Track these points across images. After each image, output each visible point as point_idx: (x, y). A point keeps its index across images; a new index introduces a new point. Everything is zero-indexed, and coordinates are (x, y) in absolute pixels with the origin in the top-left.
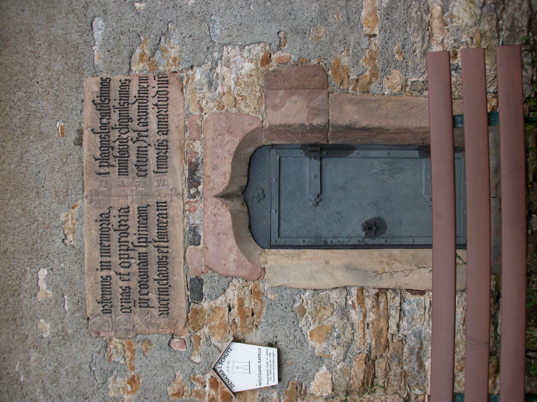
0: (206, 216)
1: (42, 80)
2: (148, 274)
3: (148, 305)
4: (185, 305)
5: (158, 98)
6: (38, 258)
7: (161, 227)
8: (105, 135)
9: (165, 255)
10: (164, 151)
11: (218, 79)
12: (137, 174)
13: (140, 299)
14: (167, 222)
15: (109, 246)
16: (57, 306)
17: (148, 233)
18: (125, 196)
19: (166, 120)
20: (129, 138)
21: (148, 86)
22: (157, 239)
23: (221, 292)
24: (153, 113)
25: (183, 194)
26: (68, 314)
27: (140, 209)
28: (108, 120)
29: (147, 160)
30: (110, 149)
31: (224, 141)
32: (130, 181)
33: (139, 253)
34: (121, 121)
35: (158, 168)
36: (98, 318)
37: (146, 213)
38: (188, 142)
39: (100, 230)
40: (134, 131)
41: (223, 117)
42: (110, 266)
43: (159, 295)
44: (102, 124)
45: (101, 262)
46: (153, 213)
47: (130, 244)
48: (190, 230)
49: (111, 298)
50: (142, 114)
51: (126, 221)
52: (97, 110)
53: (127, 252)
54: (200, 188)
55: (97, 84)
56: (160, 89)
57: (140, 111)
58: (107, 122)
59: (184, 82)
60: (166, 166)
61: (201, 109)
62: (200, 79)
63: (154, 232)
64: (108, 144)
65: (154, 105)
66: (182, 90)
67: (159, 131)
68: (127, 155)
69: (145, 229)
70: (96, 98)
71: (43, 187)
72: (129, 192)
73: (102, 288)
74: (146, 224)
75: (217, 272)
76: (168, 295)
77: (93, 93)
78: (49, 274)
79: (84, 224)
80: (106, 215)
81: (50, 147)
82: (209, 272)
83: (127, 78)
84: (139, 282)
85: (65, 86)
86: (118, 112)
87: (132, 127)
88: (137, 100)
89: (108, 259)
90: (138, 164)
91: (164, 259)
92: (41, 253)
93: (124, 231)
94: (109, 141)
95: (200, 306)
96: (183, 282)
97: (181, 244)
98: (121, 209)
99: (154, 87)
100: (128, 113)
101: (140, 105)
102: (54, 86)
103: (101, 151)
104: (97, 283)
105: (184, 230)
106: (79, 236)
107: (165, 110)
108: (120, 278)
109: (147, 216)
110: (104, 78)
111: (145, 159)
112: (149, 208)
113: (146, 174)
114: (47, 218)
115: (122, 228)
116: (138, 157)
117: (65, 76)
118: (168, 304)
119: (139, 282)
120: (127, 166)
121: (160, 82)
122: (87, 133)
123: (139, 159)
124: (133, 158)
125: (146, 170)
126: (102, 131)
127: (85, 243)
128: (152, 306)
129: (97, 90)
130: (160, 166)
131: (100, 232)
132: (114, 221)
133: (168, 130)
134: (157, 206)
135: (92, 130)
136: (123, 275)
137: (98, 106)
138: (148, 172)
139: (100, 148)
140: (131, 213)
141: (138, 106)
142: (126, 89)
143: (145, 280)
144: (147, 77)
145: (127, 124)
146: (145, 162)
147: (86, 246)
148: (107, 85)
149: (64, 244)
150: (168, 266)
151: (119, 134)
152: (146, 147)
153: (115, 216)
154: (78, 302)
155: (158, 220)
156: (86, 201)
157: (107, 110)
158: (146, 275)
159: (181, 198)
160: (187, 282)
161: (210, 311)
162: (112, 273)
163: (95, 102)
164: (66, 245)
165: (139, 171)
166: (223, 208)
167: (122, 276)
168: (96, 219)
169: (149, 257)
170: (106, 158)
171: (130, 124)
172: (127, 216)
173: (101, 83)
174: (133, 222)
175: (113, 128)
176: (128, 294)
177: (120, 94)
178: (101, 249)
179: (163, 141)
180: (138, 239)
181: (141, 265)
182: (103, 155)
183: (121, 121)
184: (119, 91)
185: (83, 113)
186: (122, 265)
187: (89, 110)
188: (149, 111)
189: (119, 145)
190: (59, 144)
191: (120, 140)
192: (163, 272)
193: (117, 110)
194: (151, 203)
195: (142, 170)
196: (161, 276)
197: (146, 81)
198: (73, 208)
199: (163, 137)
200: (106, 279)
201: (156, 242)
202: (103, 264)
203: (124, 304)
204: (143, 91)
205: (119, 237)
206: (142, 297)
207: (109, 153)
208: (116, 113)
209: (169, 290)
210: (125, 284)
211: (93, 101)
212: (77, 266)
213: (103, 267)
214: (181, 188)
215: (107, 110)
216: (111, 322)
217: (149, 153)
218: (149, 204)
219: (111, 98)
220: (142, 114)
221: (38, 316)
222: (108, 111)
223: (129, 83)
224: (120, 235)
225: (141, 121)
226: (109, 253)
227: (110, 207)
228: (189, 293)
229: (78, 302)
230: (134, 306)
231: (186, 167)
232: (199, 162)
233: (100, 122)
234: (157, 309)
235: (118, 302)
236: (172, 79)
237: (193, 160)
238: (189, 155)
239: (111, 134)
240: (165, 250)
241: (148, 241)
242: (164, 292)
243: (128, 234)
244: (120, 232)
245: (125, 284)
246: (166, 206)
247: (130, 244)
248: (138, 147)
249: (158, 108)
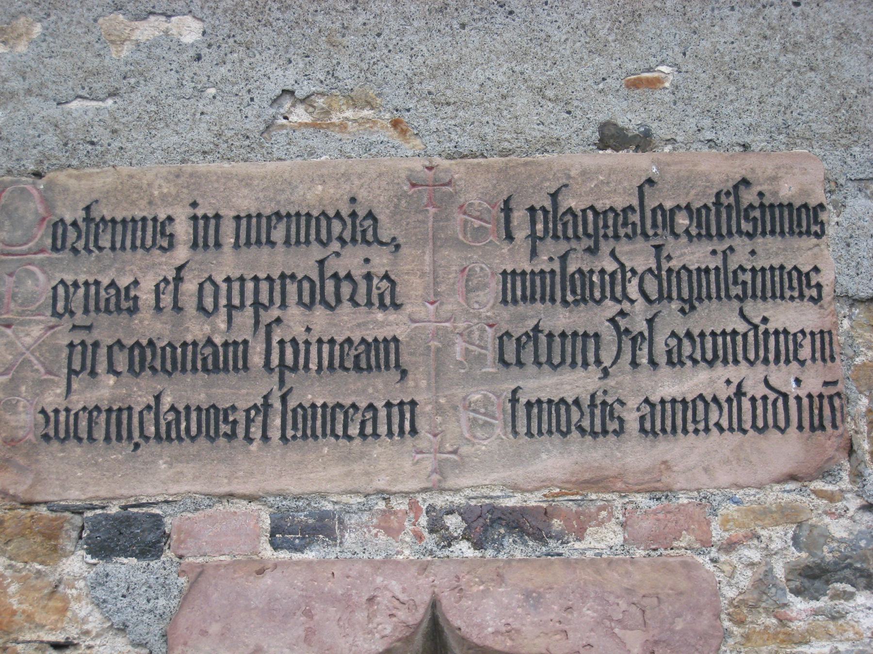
0: (368, 570)
1: (805, 16)
2: (177, 375)
3: (77, 373)
4: (74, 496)
5: (765, 398)
6: (233, 13)
7: (333, 419)
8: (634, 224)
9: (241, 431)
10: (586, 424)
11: (832, 598)
12: (508, 334)
13: (96, 345)
14: (350, 438)
15: (271, 243)
16: (81, 75)
17: (313, 374)
18: (436, 294)
19: (691, 427)
20: (626, 306)
21: (802, 363)
22: (292, 404)
23: (116, 619)
24: (712, 381)
25: (442, 490)
26: (55, 112)
27: (392, 345)
28: (687, 232)
29: (555, 367)
30: (591, 243)
31: (625, 628)
32: (486, 312)
33: (245, 342)
34: (684, 275)
35: (529, 405)
36: (41, 210)
37: (378, 367)
38: (619, 503)
39: (324, 213)
40: (650, 322)
41: (704, 622)
42: (206, 246)
43: (109, 410)
44: (672, 211)
45: (217, 217)
46: (376, 389)
47: (275, 312)
48: (323, 516)
49: (100, 249)
50: (709, 345)
51: (352, 299)
52: (718, 195)
53: (249, 301)
54: (464, 549)
55: (803, 192)
56: (792, 403)
57: (720, 340)
58: (679, 230)
59: (818, 485)
60: (535, 430)
61: (730, 546)
62: (833, 539)
63: (313, 392)
64: (606, 236)
65: (740, 386)
66: (793, 478)
67: (653, 406)
68: (570, 298)
69: (326, 363)
70: (756, 189)
71: (463, 26)
72: (449, 307)
73: (133, 220)
74: (343, 367)
75: (181, 606)
76: (107, 439)
77: (774, 179)
78: (182, 48)
79: (343, 160)
80: (370, 232)
81: (593, 45)
82: (183, 580)
83: (826, 290)
84: (151, 343)
85: (792, 91)
86: (712, 266)
87: (665, 312)
88: (756, 327)
89: (229, 240)
90: (543, 338)
91: (224, 428)
92: (251, 22)
93: (318, 293)
94: (616, 237)
95: (70, 547)
96: (151, 491)
97: (274, 486)
98: (393, 283)
99: (798, 381)
100: (709, 297)
101: (739, 339)
102: (790, 56)
103: (584, 211)
104: (150, 203)
105: (324, 496)
106: (303, 143)
107: (725, 424)
108: (165, 280)
109: (369, 368)
110: (823, 216)
111: (557, 360)
112: (395, 375)
113: (506, 364)
114: (361, 40)
115: (330, 286)
116: (563, 335)
117: (822, 87)
118: (80, 440)
119: (151, 343)
120: (533, 299)
121: (816, 400)
122: (641, 163)
123: (558, 339)
124: (561, 319)
125: (520, 363)
126: (648, 214)
127: (279, 163)
128: (75, 386)
129: (781, 194)
130: (535, 410)
131: (315, 213)
132: (350, 261)
133: (655, 434)
134: (401, 404)
135: (650, 181)
136: (176, 289)
137: (732, 199)
138: (515, 370)
139: (592, 208)
140: (380, 316)
141: (734, 333)
142: (791, 288)
143: (158, 365)
144: (833, 359)
145: (675, 295)
146: (549, 361)
147: (271, 166)
148: (799, 225)
149: (279, 97)
150: (202, 441)
151: (640, 270)
152: (598, 362)
153: (367, 261)
154: (92, 143)
155: (354, 406)
156: (418, 165)
157: (719, 228)
158: (174, 367)
159: (429, 485)
160: (148, 505)
161: (53, 578)
162: (182, 253)
163: (742, 187)
164: (274, 101)
165: (518, 340)
166: (395, 629)
167: (171, 287)
168: (360, 198)
169: (232, 378)
170: (560, 227)
171: (675, 305)
172: (369, 304)
173: (805, 206)
174: (350, 323)
175: (658, 248)
176: (112, 306)
177: (772, 268)
178: (259, 216)
179: (621, 421)
180: (294, 341)
181: (208, 351)
182: (569, 217)
183: (684, 275)
184: (782, 268)
185: (705, 149)
186: (208, 287)
187: (716, 169)
188: (719, 368)
189: (602, 272)
190: (603, 73)
191: (619, 276)
192: (183, 425)
193: (717, 261)
194: (411, 383)
195: (520, 350)
196: (171, 417)
197: (818, 355)
198: (396, 124)
199: (632, 420)
200: (163, 234)
201: (284, 399)
202: (213, 222)
203: (81, 291)
204: (782, 347)
205: (300, 276)
206: (103, 351)
207: (577, 237)
208: (710, 258)
209: (124, 443)
210: (146, 296)
211: (745, 182)
212: (207, 137)
213: (201, 222)
214: (463, 482)
215: (719, 228)
216: (25, 248)
217: (580, 372)
218: (410, 376)
219: (760, 240)
220: (709, 345)
221: (53, 18)
222: (714, 231)
223: (812, 299)
224: (306, 277)
225: (686, 343)
226: (248, 243)
227: (398, 247)
228: (114, 510)
229: (92, 143)
230: (75, 327)
231: (533, 500)
232: (552, 543)
233: (678, 207)
234: (62, 404)
235: (89, 272)
236: (829, 442)
237: (557, 524)
238: (574, 508)
239: (640, 243)
240: (256, 431)
241: (287, 373)
242: (118, 427)
243: (309, 307)
244: (315, 277)
245: (146, 296)
246: (402, 432)
247: (275, 312)
248: (597, 336)
249: (729, 400)
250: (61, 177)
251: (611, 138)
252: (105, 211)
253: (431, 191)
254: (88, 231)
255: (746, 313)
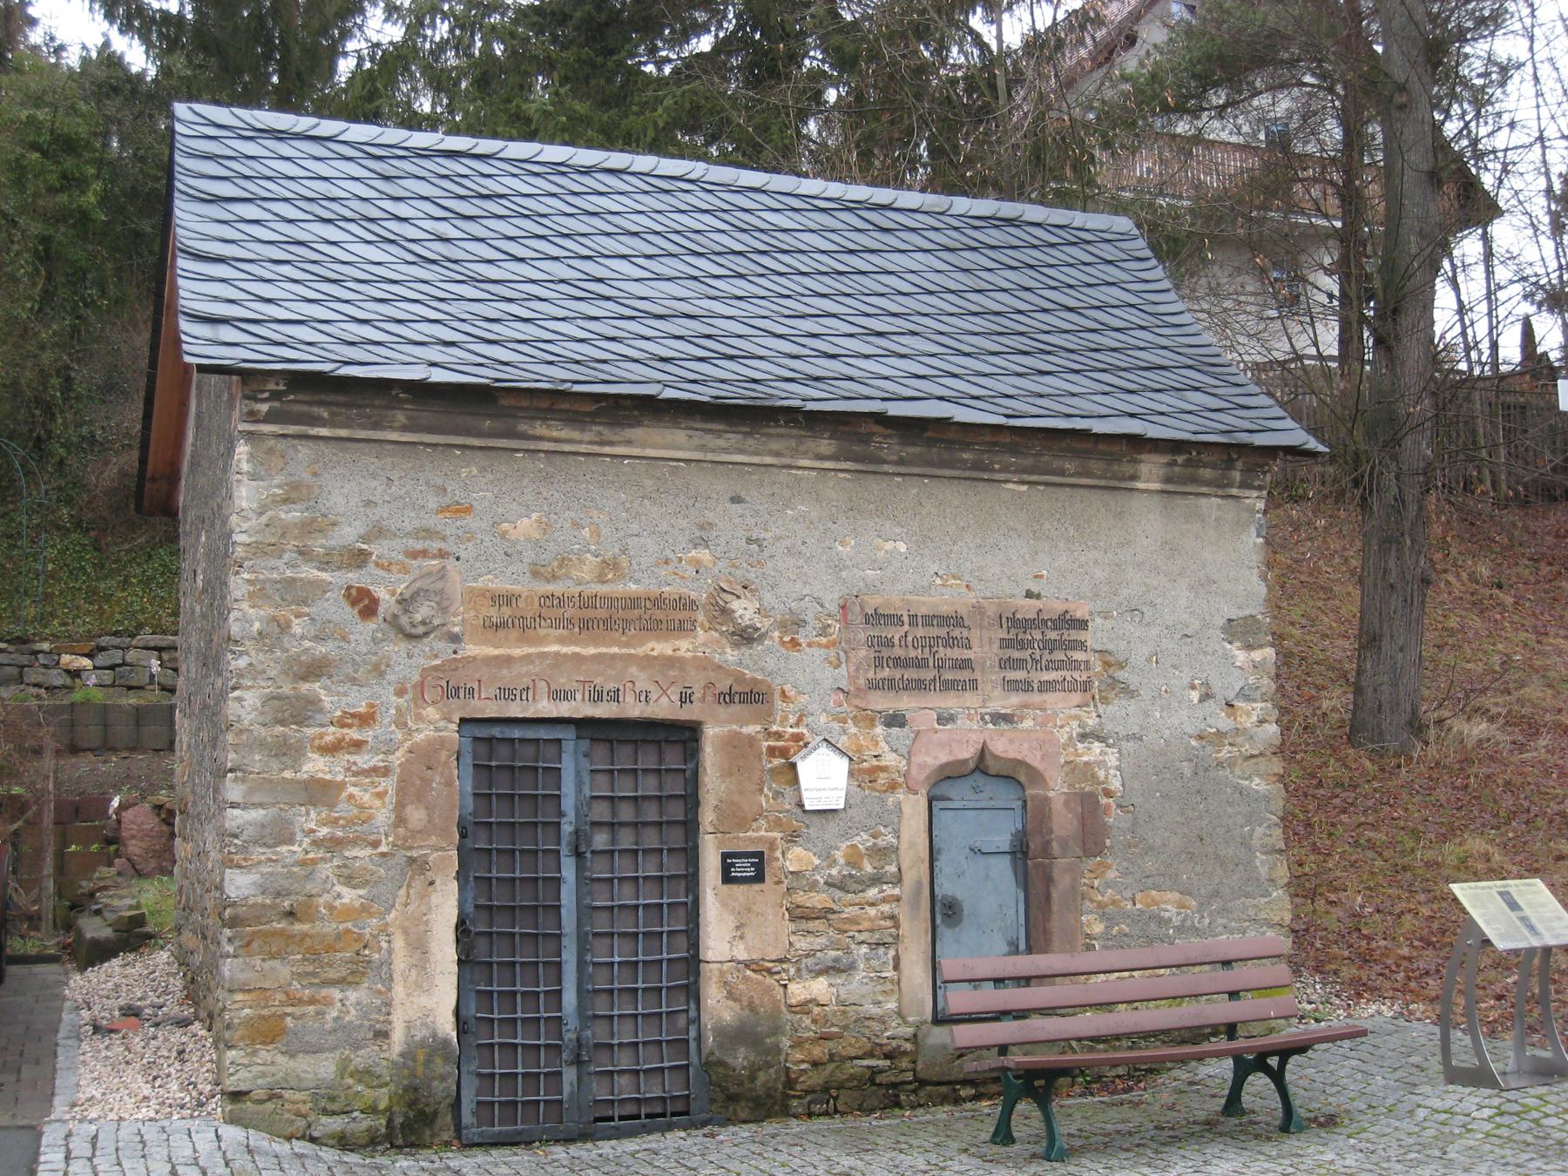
4: (879, 708)
46: (965, 675)
54: (990, 726)
93: (950, 642)
124: (1016, 654)
132: (956, 633)
162: (906, 627)
174: (957, 653)
187: (1059, 607)
195: (1006, 664)
204: (1075, 665)
210: (896, 641)
242: (890, 685)
250: (866, 598)
251: (1029, 595)
252: (881, 611)
253: (978, 609)
254: (876, 618)
255: (1280, 1113)
